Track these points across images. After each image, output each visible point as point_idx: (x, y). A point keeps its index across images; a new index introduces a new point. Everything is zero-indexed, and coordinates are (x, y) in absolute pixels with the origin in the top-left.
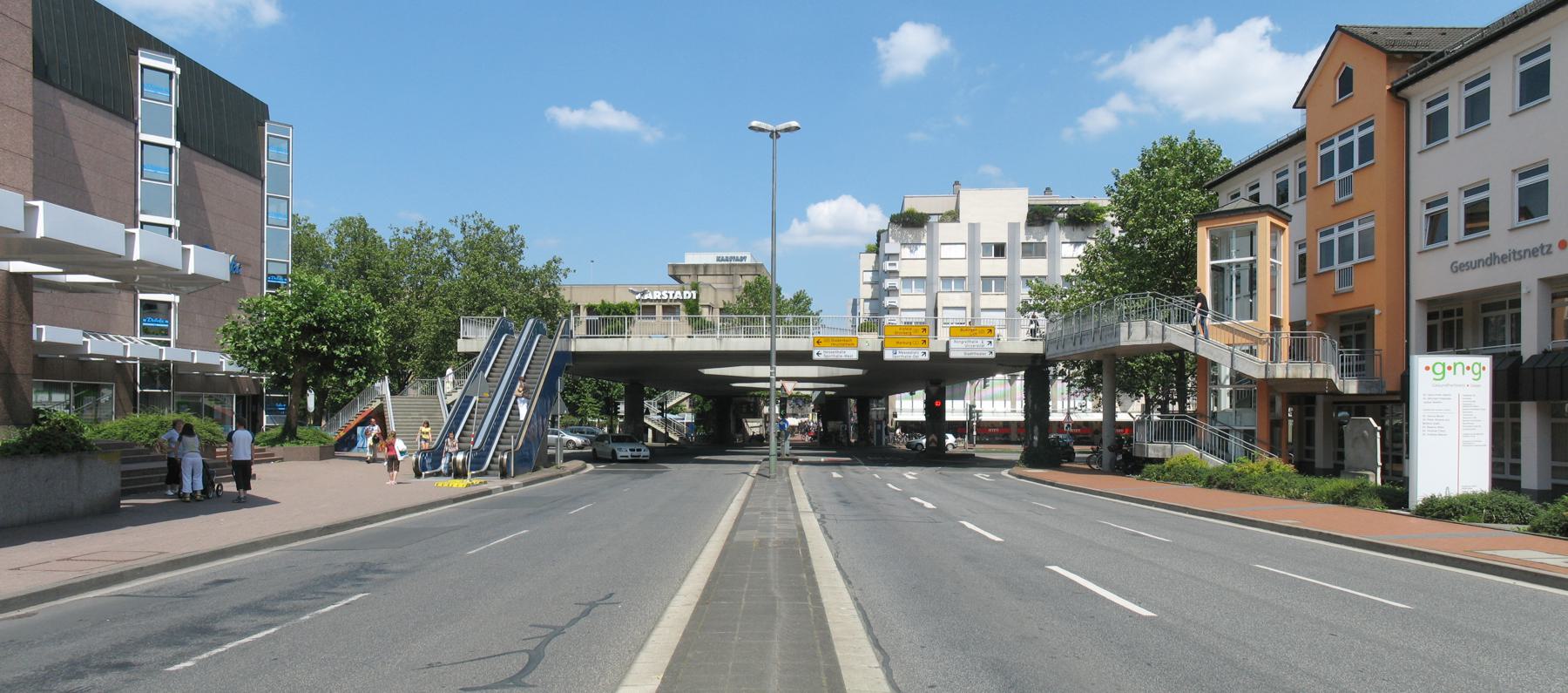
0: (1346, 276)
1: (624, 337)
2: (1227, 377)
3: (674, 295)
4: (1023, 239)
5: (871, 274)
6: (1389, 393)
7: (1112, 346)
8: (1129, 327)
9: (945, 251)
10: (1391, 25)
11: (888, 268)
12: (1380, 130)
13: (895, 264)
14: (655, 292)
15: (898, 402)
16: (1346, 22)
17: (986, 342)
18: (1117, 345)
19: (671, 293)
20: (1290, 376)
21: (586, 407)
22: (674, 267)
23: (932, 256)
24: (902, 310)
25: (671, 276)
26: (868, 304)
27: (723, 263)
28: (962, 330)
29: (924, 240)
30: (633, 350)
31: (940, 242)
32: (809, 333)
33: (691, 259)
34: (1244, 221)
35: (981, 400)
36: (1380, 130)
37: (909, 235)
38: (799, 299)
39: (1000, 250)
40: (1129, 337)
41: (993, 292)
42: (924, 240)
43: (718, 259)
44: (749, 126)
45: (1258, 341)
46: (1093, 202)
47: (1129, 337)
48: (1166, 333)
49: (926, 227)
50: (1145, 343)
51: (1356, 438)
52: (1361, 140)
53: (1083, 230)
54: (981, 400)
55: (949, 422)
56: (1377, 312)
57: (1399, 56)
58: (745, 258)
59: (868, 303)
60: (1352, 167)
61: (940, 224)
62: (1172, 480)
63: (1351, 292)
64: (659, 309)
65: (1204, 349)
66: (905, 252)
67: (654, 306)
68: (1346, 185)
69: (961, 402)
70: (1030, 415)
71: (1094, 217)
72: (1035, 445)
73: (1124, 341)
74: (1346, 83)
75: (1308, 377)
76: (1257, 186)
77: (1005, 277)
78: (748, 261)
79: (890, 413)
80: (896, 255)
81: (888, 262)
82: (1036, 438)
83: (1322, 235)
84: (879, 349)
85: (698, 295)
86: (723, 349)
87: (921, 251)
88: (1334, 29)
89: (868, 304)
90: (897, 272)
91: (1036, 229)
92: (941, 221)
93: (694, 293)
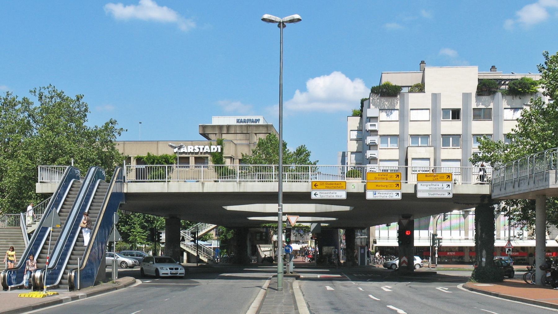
1: (165, 182)
3: (203, 149)
4: (474, 105)
5: (356, 133)
9: (414, 115)
13: (375, 125)
14: (189, 147)
18: (547, 187)
19: (201, 147)
21: (136, 236)
22: (204, 127)
23: (403, 119)
24: (381, 160)
26: (354, 156)
27: (241, 124)
29: (398, 107)
31: (410, 108)
37: (386, 102)
39: (456, 114)
42: (398, 107)
46: (528, 77)
53: (520, 99)
58: (258, 120)
61: (410, 94)
66: (383, 116)
67: (188, 158)
69: (426, 232)
71: (529, 89)
72: (483, 265)
77: (460, 135)
78: (261, 123)
79: (371, 240)
80: (376, 118)
81: (369, 124)
82: (484, 260)
85: (222, 149)
86: (242, 190)
87: (395, 115)
89: (354, 156)
90: (376, 131)
91: (485, 98)
92: (410, 92)
93: (219, 147)
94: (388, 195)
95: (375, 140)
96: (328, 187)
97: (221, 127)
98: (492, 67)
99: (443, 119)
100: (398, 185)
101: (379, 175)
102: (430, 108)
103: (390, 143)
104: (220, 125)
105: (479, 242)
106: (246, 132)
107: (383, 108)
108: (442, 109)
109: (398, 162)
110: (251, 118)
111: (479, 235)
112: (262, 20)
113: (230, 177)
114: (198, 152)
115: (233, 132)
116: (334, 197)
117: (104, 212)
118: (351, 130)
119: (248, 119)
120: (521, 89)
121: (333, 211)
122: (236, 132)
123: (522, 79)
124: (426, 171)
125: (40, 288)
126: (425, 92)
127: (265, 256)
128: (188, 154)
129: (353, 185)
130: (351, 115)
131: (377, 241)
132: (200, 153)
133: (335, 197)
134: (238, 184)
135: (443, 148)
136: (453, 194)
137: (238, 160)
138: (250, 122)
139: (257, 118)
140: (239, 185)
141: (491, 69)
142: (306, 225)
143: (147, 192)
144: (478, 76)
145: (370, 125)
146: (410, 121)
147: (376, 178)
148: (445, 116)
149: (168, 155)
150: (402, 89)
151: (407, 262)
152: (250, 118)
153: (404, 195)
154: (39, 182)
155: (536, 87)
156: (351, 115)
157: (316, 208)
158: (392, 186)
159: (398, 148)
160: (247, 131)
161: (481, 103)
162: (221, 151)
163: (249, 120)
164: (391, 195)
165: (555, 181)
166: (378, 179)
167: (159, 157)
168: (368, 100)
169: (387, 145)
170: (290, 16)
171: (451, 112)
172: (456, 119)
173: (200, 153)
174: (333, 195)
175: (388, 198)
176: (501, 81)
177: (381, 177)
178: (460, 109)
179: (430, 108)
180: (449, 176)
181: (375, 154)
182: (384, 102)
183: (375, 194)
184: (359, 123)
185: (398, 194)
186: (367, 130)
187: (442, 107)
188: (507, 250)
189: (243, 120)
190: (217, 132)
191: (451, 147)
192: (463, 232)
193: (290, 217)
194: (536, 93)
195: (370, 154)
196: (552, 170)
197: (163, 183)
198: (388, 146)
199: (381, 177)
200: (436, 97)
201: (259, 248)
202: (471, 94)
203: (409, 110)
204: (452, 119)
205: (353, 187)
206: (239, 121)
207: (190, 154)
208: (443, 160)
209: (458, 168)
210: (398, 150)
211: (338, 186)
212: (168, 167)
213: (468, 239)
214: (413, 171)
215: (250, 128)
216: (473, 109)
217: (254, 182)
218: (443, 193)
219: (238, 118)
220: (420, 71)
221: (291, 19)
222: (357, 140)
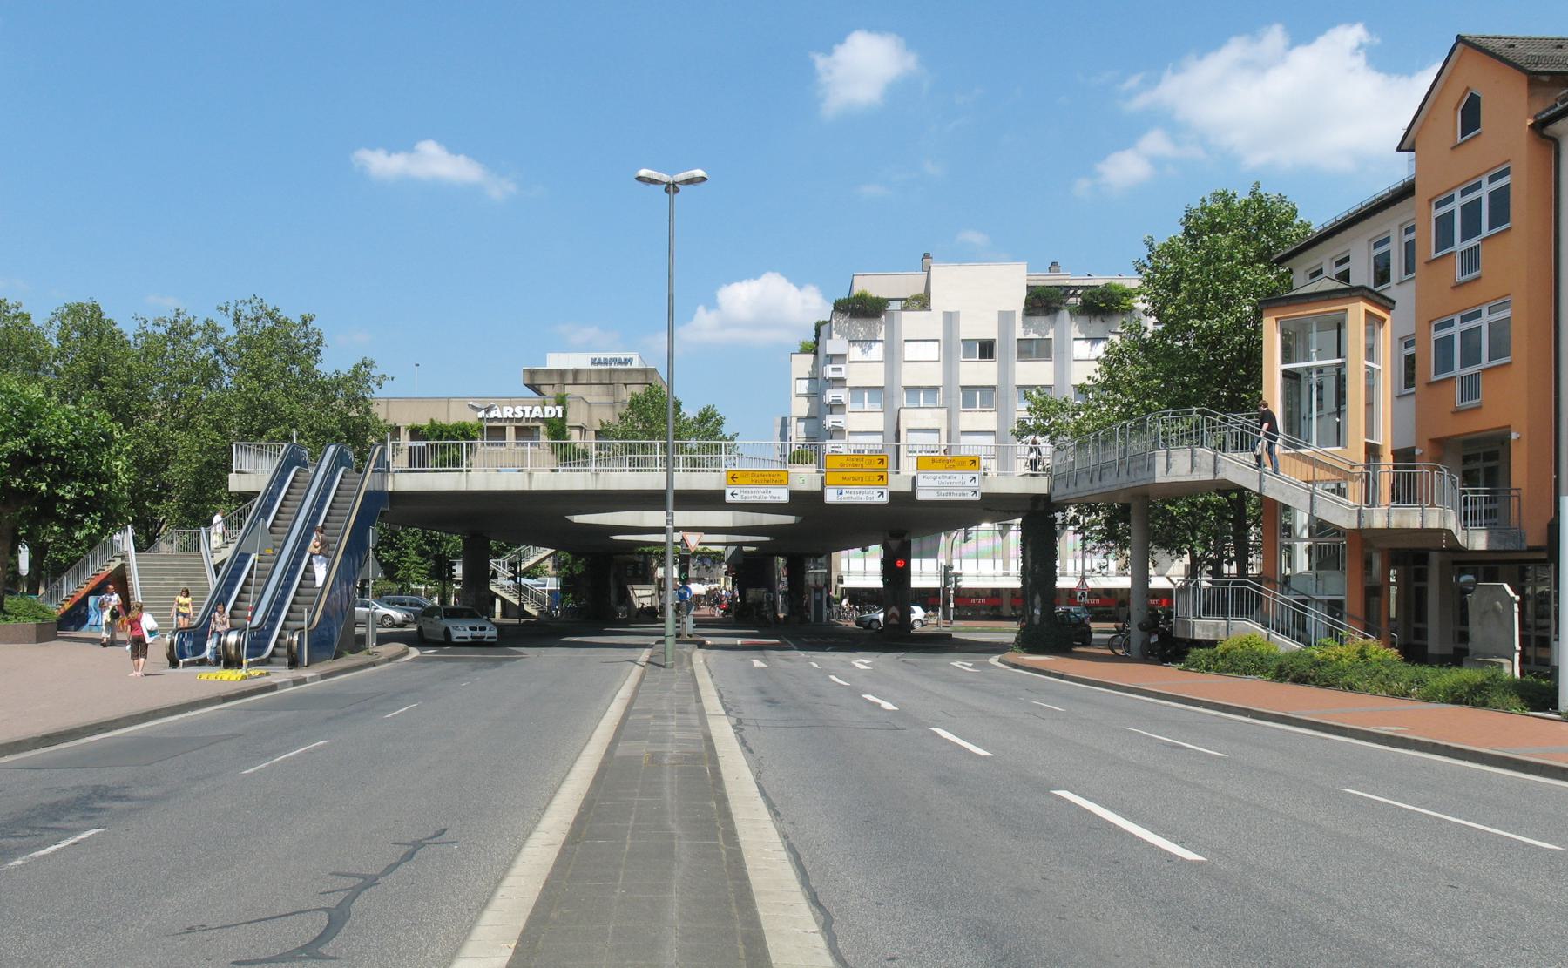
0: (1471, 386)
1: (462, 471)
2: (1304, 527)
3: (531, 412)
4: (1019, 333)
5: (806, 382)
6: (1531, 549)
7: (1143, 483)
9: (911, 351)
12: (1519, 183)
13: (840, 369)
15: (844, 563)
16: (1472, 31)
18: (1152, 481)
19: (527, 409)
20: (1393, 526)
22: (532, 373)
23: (892, 358)
25: (526, 385)
26: (802, 425)
27: (599, 367)
29: (882, 336)
33: (555, 362)
37: (860, 328)
39: (987, 349)
41: (978, 408)
42: (882, 336)
45: (1347, 476)
46: (1117, 282)
48: (1219, 465)
49: (883, 317)
50: (1189, 479)
52: (1492, 195)
56: (1514, 436)
57: (1545, 78)
58: (630, 360)
61: (903, 313)
63: (1478, 408)
66: (855, 352)
67: (504, 428)
68: (1471, 259)
70: (1029, 580)
71: (1118, 303)
72: (1037, 621)
73: (1161, 476)
74: (1471, 115)
75: (1418, 526)
77: (994, 387)
78: (635, 365)
79: (834, 577)
82: (1037, 612)
85: (564, 413)
86: (600, 487)
87: (877, 351)
88: (1455, 41)
89: (802, 425)
90: (842, 380)
91: (1039, 320)
92: (905, 309)
93: (559, 409)
94: (864, 496)
97: (562, 373)
102: (941, 338)
103: (869, 402)
104: (560, 370)
106: (608, 382)
108: (962, 340)
109: (881, 436)
110: (618, 357)
115: (584, 382)
118: (798, 379)
119: (611, 359)
122: (589, 382)
124: (933, 452)
131: (845, 578)
132: (524, 420)
136: (791, 491)
140: (596, 478)
141: (1050, 268)
146: (905, 362)
147: (842, 465)
148: (968, 353)
152: (614, 356)
153: (892, 495)
154: (234, 471)
155: (1131, 300)
157: (734, 518)
160: (610, 380)
163: (613, 360)
171: (978, 345)
173: (524, 420)
174: (764, 495)
178: (995, 340)
179: (941, 338)
183: (841, 494)
185: (882, 493)
190: (555, 382)
194: (1131, 311)
196: (1160, 450)
198: (864, 407)
200: (950, 319)
201: (631, 592)
204: (980, 358)
205: (801, 481)
208: (963, 433)
210: (882, 414)
214: (910, 452)
215: (616, 373)
216: (1019, 340)
218: (965, 492)
219: (594, 357)
222: (809, 396)
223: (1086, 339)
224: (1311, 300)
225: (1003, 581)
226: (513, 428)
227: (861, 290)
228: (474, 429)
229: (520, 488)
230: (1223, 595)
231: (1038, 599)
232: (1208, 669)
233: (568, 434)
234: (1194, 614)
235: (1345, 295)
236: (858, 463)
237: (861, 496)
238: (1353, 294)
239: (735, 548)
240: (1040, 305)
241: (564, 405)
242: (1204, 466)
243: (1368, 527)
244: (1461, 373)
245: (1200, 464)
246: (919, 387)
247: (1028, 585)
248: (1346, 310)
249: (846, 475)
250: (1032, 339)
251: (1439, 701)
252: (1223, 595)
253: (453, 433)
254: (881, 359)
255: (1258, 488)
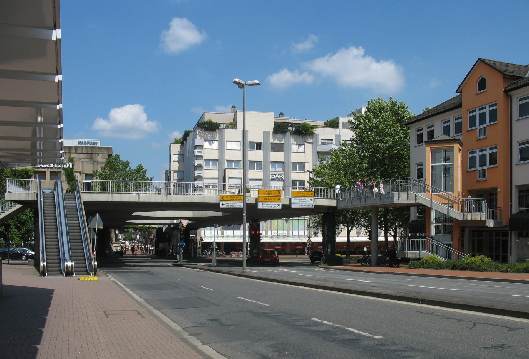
0: (483, 174)
1: (109, 193)
2: (434, 219)
4: (271, 140)
5: (177, 156)
6: (504, 227)
7: (388, 203)
8: (399, 194)
9: (229, 145)
10: (498, 61)
11: (197, 154)
12: (500, 109)
13: (201, 152)
15: (202, 232)
16: (482, 57)
17: (310, 199)
18: (392, 203)
20: (473, 219)
21: (12, 234)
23: (222, 148)
24: (205, 178)
26: (176, 174)
27: (82, 145)
28: (298, 193)
29: (217, 139)
30: (173, 201)
31: (226, 140)
32: (110, 191)
34: (439, 146)
35: (299, 230)
36: (500, 109)
37: (209, 135)
38: (139, 169)
39: (259, 146)
40: (398, 200)
41: (255, 170)
42: (217, 139)
43: (79, 143)
44: (234, 81)
45: (454, 202)
46: (307, 122)
47: (398, 200)
48: (417, 197)
49: (218, 131)
50: (406, 202)
51: (523, 246)
52: (490, 112)
53: (303, 137)
54: (299, 230)
55: (338, 242)
56: (499, 190)
57: (508, 77)
58: (96, 143)
59: (176, 173)
60: (486, 123)
61: (226, 130)
62: (429, 268)
63: (486, 181)
64: (48, 174)
65: (435, 206)
66: (206, 145)
67: (45, 172)
68: (483, 132)
69: (238, 231)
70: (326, 238)
71: (308, 131)
72: (329, 253)
73: (396, 201)
74: (482, 84)
75: (479, 219)
76: (433, 126)
77: (262, 162)
78: (98, 145)
79: (198, 238)
80: (201, 147)
81: (197, 150)
82: (329, 250)
83: (470, 153)
84: (255, 203)
85: (73, 166)
86: (168, 201)
87: (215, 145)
88: (477, 60)
89: (176, 174)
90: (202, 156)
91: (278, 136)
92: (226, 128)
93: (71, 164)
94: (273, 206)
95: (201, 163)
96: (232, 199)
97: (70, 148)
98: (281, 113)
99: (250, 149)
100: (279, 198)
101: (266, 192)
102: (241, 141)
103: (212, 165)
104: (69, 146)
105: (326, 238)
106: (91, 152)
107: (206, 139)
108: (249, 142)
109: (217, 180)
110: (91, 141)
111: (326, 233)
112: (233, 82)
113: (141, 190)
114: (53, 167)
116: (236, 207)
117: (85, 217)
118: (174, 154)
119: (87, 142)
120: (303, 131)
121: (208, 216)
122: (82, 152)
123: (303, 123)
124: (232, 187)
125: (70, 274)
126: (237, 129)
127: (117, 251)
128: (45, 169)
129: (248, 198)
130: (173, 143)
131: (203, 238)
132: (54, 168)
133: (237, 207)
134: (166, 196)
135: (250, 171)
136: (282, 205)
137: (84, 174)
138: (89, 144)
139: (95, 141)
140: (166, 197)
141: (279, 115)
142: (154, 227)
143: (96, 201)
144: (274, 119)
145: (198, 151)
146: (227, 150)
147: (264, 194)
148: (252, 148)
149: (27, 169)
150: (220, 126)
151: (257, 253)
152: (89, 141)
153: (283, 205)
154: (7, 191)
155: (313, 130)
156: (173, 143)
157: (194, 214)
158: (275, 199)
159: (217, 169)
161: (276, 139)
162: (72, 167)
163: (88, 143)
164: (275, 206)
165: (398, 199)
166: (266, 194)
167: (20, 170)
168: (193, 132)
169: (209, 166)
170: (252, 81)
171: (255, 144)
172: (258, 150)
173: (54, 168)
174: (235, 205)
175: (273, 207)
176: (288, 124)
177: (268, 193)
178: (262, 142)
179: (241, 141)
180: (279, 192)
181: (201, 174)
182: (207, 134)
183: (264, 205)
184: (180, 149)
185: (279, 205)
186: (195, 155)
187: (249, 141)
188: (308, 244)
189: (93, 142)
190: (67, 152)
191: (255, 170)
192: (286, 232)
193: (182, 221)
194: (313, 134)
195: (198, 173)
196: (395, 192)
197: (108, 194)
198: (210, 168)
199: (268, 193)
200: (244, 133)
201: (111, 244)
202: (269, 132)
203: (226, 141)
204: (256, 150)
205: (248, 200)
206: (81, 143)
207: (46, 169)
208: (250, 180)
209: (260, 185)
210: (218, 171)
211: (239, 199)
212: (112, 182)
213: (223, 237)
214: (230, 187)
215: (95, 149)
216: (271, 143)
217: (160, 195)
218: (309, 205)
219: (80, 141)
220: (232, 113)
221: (253, 83)
222: (179, 162)
223: (296, 144)
224: (442, 142)
225: (266, 239)
226: (49, 172)
227: (209, 119)
228: (31, 172)
229: (134, 201)
230: (418, 242)
231: (329, 245)
232: (420, 267)
233: (74, 175)
234: (408, 249)
235: (453, 141)
236: (270, 193)
237: (271, 206)
238: (456, 141)
239: (168, 226)
240: (279, 130)
241: (73, 162)
242: (412, 198)
243: (466, 219)
244: (479, 169)
245: (410, 197)
246: (232, 160)
247: (326, 240)
248: (453, 146)
249: (265, 198)
250: (276, 143)
251: (521, 272)
252: (418, 242)
253: (21, 173)
254: (217, 148)
255: (430, 206)
